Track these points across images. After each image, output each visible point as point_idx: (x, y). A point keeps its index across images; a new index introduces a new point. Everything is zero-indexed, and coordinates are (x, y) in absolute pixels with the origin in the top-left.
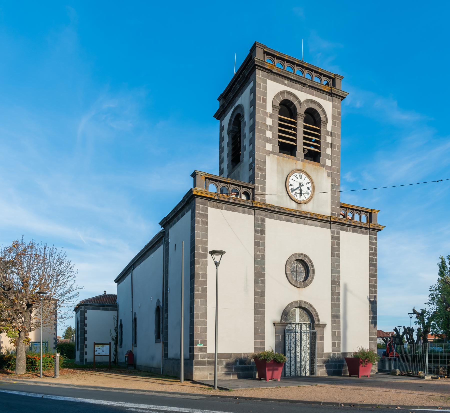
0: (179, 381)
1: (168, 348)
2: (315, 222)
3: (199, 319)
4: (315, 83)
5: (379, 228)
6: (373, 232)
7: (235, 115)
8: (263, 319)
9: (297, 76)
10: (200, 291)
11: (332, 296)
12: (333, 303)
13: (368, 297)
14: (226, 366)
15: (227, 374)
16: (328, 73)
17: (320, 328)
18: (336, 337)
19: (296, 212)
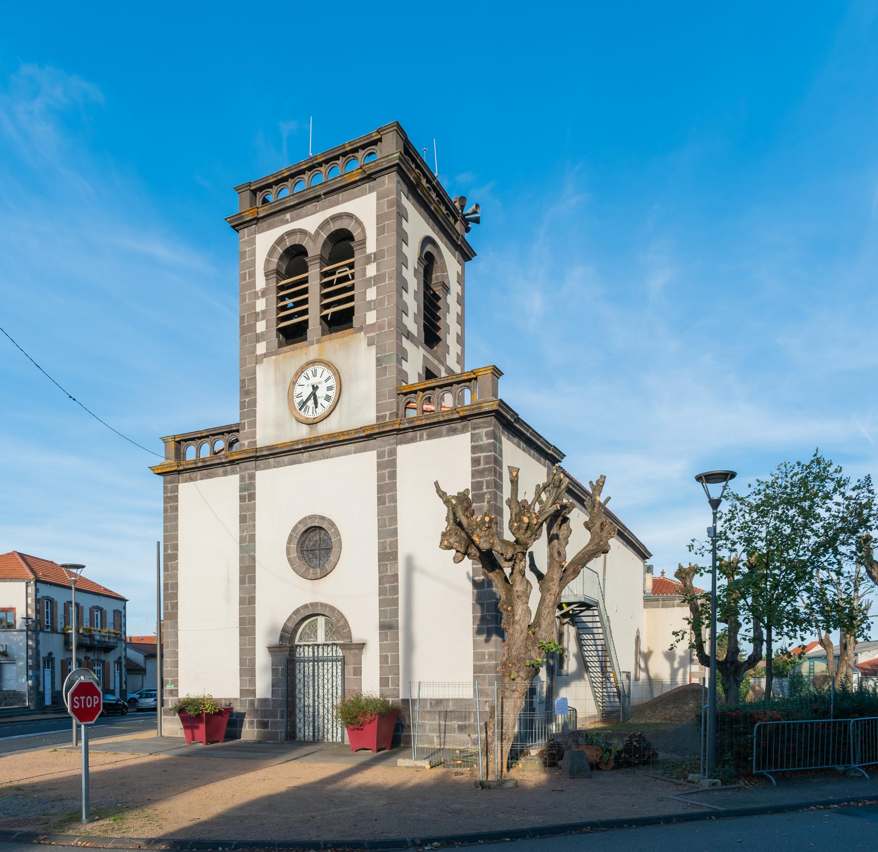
2: (345, 446)
4: (330, 183)
6: (481, 420)
9: (297, 195)
11: (380, 584)
12: (382, 597)
13: (468, 573)
16: (365, 138)
17: (352, 651)
18: (388, 667)
19: (298, 444)
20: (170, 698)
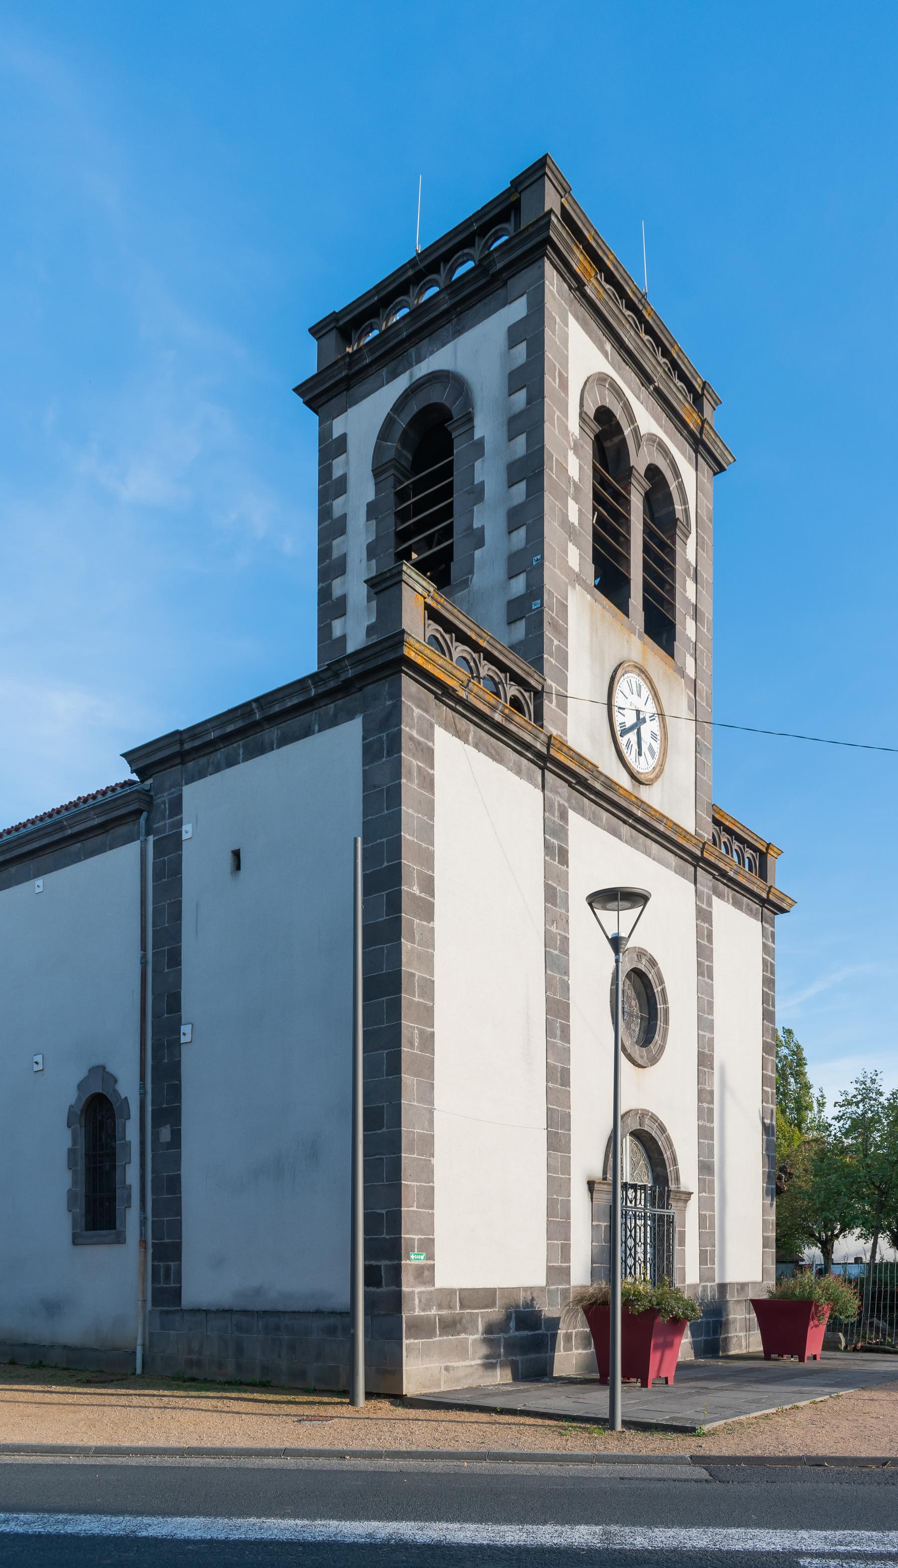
0: (348, 1400)
1: (180, 1265)
3: (415, 1156)
5: (784, 905)
7: (414, 407)
8: (566, 1169)
10: (416, 1044)
14: (485, 1336)
15: (489, 1366)
19: (638, 807)
20: (417, 1290)
